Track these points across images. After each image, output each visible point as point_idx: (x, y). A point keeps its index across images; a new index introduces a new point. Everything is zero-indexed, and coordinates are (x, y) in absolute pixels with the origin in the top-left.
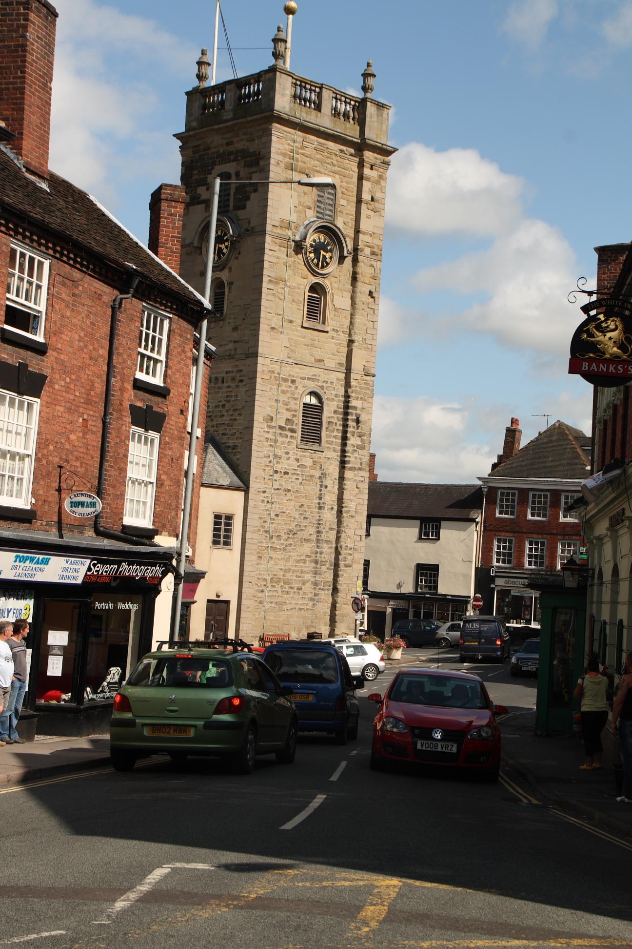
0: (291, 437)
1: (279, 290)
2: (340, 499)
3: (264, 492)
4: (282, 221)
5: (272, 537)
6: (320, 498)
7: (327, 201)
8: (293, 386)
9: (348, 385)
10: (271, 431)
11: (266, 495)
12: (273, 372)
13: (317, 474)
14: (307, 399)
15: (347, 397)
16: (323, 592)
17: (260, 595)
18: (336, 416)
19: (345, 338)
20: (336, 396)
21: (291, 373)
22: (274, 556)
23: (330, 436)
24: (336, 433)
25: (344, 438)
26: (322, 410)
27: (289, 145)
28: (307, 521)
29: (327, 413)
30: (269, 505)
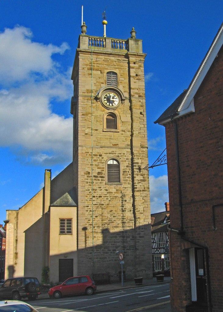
0: (102, 180)
1: (89, 118)
2: (134, 205)
3: (88, 206)
4: (88, 90)
5: (94, 227)
6: (123, 207)
7: (113, 80)
8: (100, 157)
9: (132, 153)
10: (89, 178)
11: (88, 208)
12: (88, 152)
13: (120, 195)
14: (111, 162)
15: (132, 159)
16: (129, 251)
17: (90, 255)
18: (128, 168)
19: (130, 133)
20: (127, 159)
21: (99, 152)
22: (96, 236)
23: (125, 178)
24: (129, 176)
25: (133, 178)
26: (119, 166)
27: (89, 61)
28: (116, 218)
29: (122, 168)
30: (91, 212)
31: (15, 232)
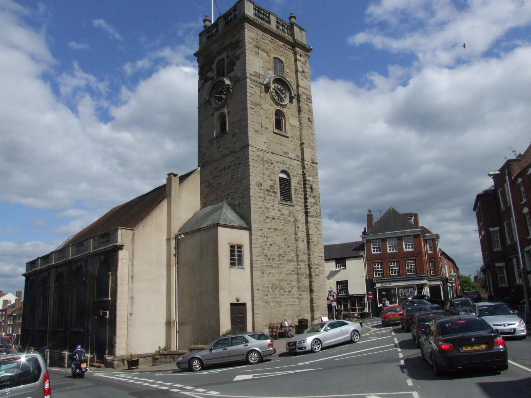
1: (258, 110)
2: (308, 235)
3: (261, 230)
5: (269, 259)
6: (296, 234)
9: (303, 168)
10: (262, 192)
13: (292, 219)
16: (304, 293)
17: (266, 297)
24: (300, 196)
30: (265, 239)
31: (131, 263)
